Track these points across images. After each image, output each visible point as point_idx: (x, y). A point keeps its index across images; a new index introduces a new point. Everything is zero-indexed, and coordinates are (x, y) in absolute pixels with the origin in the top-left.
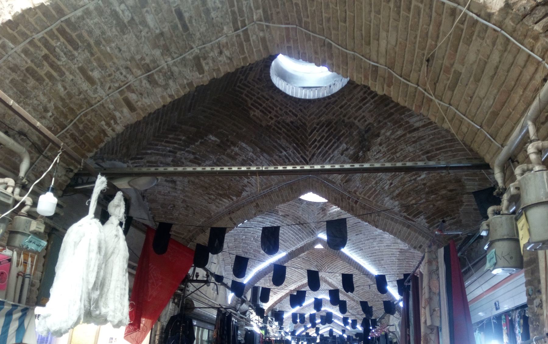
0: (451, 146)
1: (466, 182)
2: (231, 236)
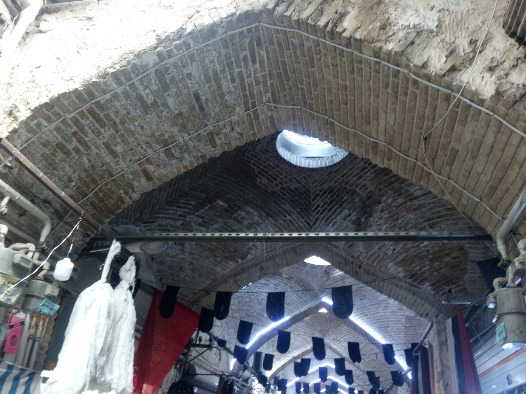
0: (451, 215)
1: (469, 250)
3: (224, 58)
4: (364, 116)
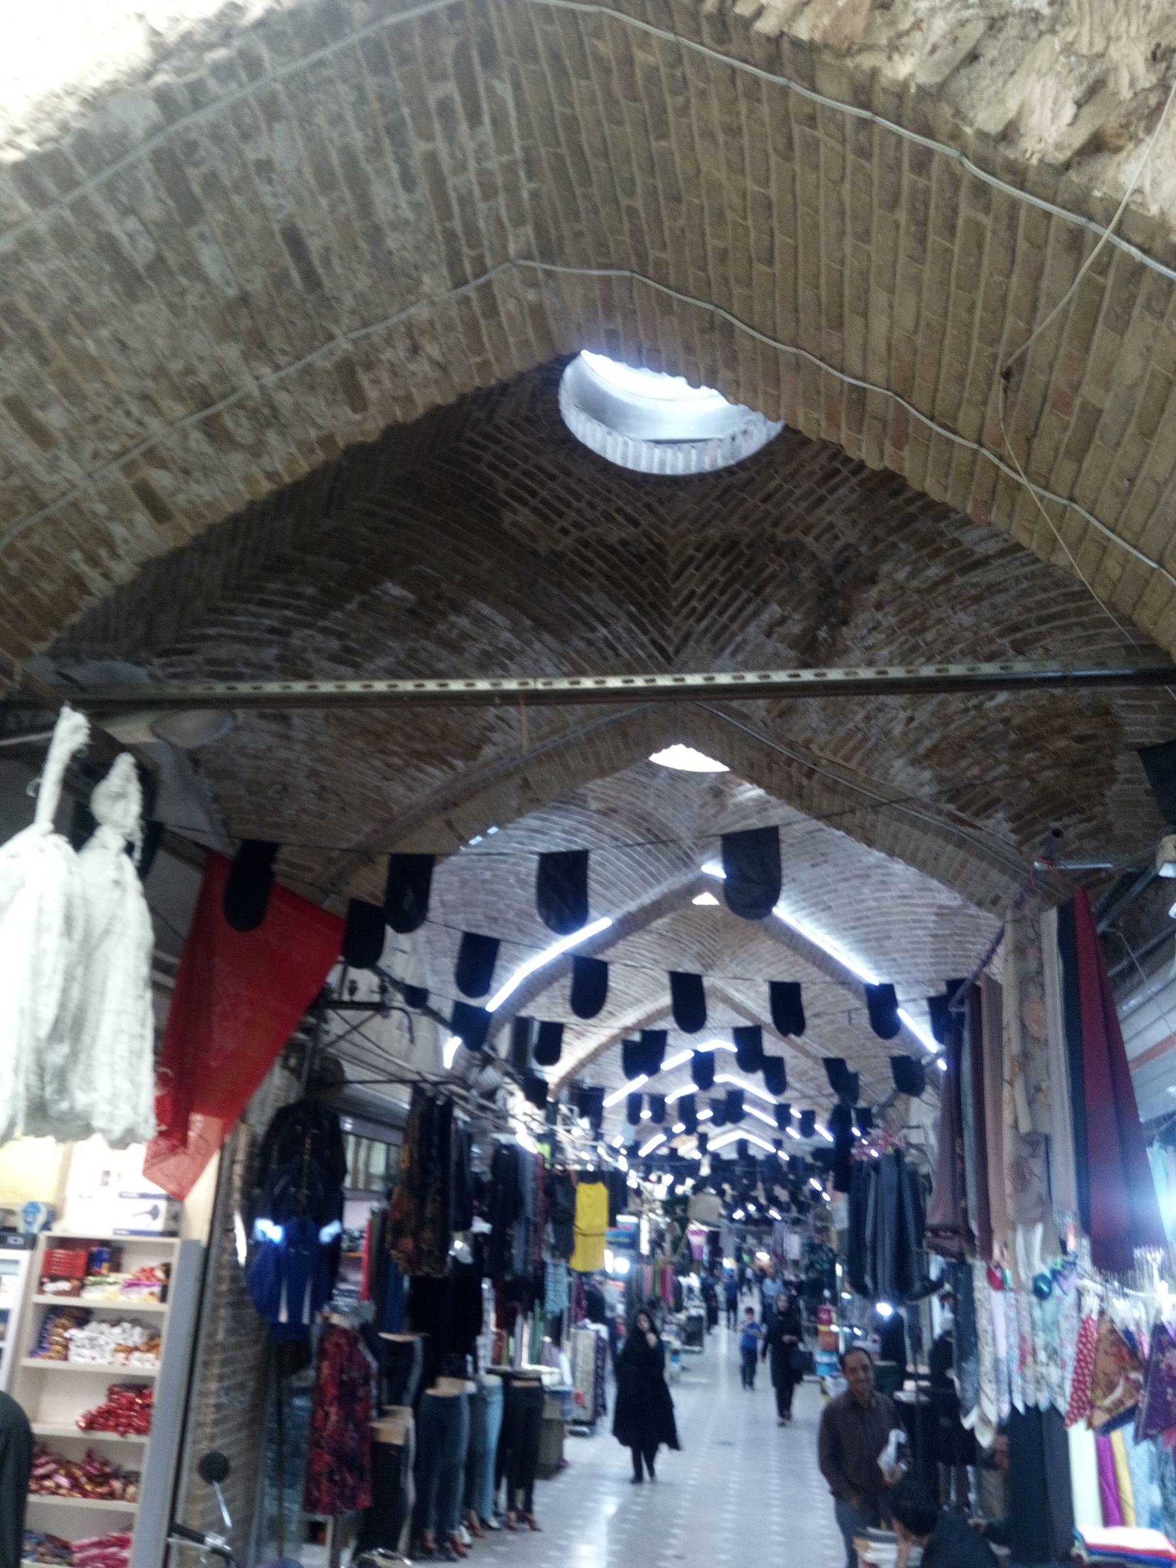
2: (452, 873)
3: (376, 106)
4: (824, 300)
